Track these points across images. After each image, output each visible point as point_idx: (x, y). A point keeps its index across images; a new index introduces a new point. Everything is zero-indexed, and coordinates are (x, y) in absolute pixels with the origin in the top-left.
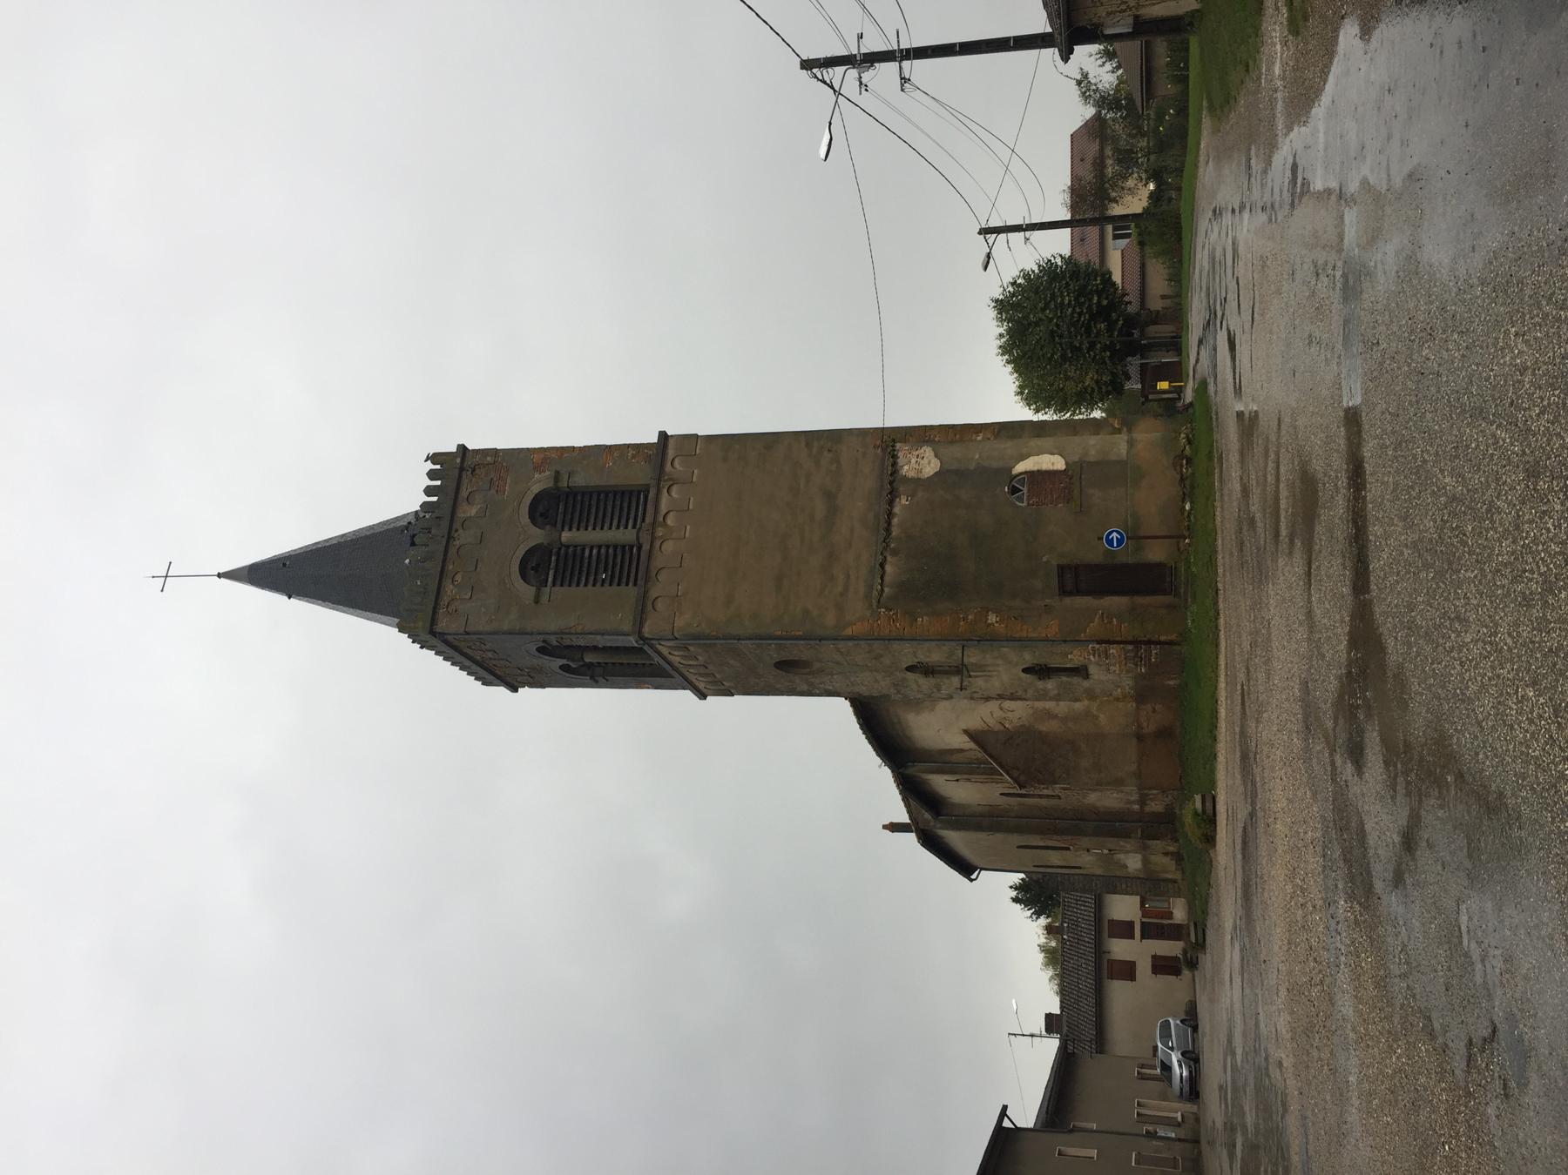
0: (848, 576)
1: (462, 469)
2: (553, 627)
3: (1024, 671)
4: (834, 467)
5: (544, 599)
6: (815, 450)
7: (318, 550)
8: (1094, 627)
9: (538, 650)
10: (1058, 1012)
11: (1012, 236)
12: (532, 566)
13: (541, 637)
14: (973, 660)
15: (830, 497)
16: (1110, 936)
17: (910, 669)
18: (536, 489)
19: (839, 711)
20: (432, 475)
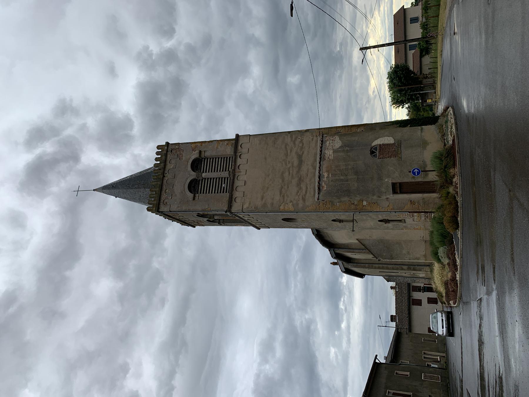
0: (307, 188)
1: (167, 151)
2: (200, 209)
4: (301, 145)
5: (197, 198)
6: (293, 139)
8: (408, 207)
10: (395, 315)
11: (372, 50)
12: (192, 184)
14: (358, 218)
16: (413, 305)
17: (334, 220)
18: (193, 157)
20: (157, 153)
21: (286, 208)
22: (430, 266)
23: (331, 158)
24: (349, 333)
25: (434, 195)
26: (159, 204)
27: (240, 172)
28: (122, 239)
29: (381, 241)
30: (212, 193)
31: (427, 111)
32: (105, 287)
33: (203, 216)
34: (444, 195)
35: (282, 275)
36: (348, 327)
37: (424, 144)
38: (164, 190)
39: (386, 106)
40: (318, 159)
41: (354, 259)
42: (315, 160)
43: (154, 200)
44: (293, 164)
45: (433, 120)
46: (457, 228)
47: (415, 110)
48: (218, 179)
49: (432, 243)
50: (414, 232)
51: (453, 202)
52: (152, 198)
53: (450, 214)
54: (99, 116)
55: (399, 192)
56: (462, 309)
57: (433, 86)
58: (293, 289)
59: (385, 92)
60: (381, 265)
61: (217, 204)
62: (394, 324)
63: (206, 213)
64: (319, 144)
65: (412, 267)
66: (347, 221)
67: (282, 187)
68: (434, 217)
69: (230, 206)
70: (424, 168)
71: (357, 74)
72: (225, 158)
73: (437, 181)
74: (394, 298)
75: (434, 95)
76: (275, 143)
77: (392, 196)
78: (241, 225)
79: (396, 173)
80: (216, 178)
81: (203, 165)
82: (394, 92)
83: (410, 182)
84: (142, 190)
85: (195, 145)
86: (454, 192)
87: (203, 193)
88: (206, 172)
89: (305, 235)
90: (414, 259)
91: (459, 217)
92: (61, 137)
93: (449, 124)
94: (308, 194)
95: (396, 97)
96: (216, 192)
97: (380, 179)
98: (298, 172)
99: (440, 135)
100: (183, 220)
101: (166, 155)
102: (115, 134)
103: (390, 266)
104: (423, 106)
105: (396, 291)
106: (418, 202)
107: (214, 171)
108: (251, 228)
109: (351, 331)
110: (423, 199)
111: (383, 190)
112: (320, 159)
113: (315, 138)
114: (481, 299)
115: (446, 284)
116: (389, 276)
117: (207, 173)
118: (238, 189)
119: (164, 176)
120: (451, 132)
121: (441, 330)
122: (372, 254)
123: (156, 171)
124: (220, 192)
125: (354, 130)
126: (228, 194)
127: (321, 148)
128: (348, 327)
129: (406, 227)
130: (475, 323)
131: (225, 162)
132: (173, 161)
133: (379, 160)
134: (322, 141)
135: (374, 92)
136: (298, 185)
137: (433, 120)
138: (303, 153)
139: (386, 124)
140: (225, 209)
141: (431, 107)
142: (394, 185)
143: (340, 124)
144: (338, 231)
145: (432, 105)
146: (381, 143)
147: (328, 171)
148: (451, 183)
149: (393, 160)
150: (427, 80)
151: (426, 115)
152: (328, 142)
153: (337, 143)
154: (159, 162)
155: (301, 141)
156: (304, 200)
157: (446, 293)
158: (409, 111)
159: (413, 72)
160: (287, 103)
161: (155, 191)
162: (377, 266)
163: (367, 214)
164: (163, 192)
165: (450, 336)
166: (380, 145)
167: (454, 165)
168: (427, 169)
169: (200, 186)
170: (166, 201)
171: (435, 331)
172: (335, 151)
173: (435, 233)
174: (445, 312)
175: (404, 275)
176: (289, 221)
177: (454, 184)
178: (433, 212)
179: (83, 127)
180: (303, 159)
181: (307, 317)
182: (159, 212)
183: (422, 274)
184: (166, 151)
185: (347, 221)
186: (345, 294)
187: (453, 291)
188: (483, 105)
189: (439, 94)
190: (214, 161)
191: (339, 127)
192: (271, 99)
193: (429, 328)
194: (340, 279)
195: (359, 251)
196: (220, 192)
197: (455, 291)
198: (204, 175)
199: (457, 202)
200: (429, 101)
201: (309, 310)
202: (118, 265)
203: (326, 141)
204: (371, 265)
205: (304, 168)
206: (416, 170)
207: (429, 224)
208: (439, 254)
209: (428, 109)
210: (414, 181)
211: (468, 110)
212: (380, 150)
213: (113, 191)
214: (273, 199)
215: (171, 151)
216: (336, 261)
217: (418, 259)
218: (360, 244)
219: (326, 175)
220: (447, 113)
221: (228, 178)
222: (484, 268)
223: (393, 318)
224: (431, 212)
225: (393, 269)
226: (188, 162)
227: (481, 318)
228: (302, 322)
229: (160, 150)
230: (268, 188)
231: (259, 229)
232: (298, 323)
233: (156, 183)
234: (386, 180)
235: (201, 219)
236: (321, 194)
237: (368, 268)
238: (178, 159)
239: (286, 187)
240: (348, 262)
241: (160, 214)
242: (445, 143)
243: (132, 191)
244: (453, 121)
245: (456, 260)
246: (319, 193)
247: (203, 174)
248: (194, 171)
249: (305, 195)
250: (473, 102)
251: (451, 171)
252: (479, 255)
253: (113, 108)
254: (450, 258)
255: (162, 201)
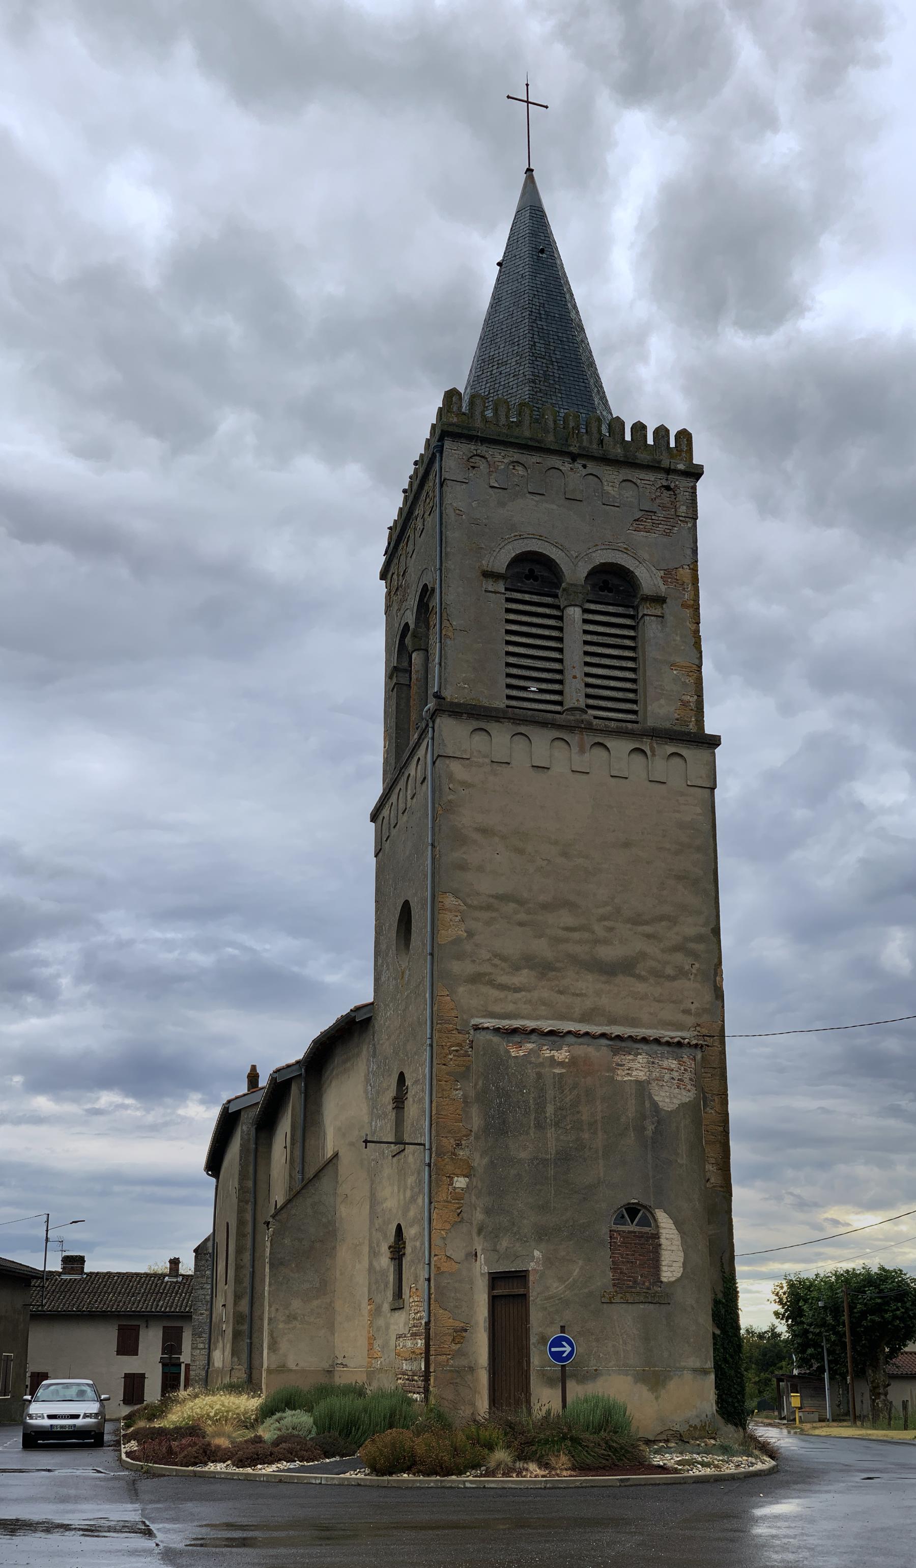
0: (517, 990)
1: (668, 471)
3: (399, 1228)
4: (669, 971)
5: (490, 585)
6: (692, 945)
7: (563, 295)
8: (446, 1321)
9: (425, 585)
13: (437, 586)
14: (411, 1159)
15: (625, 967)
16: (121, 1329)
17: (402, 1078)
19: (372, 1000)
20: (662, 432)
21: (448, 916)
22: (250, 1385)
23: (621, 1076)
24: (19, 1121)
25: (483, 1404)
26: (470, 438)
27: (582, 751)
28: (321, 286)
29: (330, 1233)
30: (508, 643)
31: (760, 1392)
32: (139, 210)
33: (424, 608)
34: (484, 1434)
35: (207, 897)
36: (38, 1120)
37: (654, 1378)
38: (523, 458)
39: (784, 1260)
40: (616, 1030)
41: (270, 1145)
42: (613, 1021)
43: (485, 420)
44: (606, 942)
45: (733, 1408)
46: (377, 1470)
47: (765, 1355)
48: (556, 666)
49: (324, 1391)
50: (364, 1335)
51: (461, 1461)
52: (496, 410)
53: (420, 1450)
54: (803, 185)
55: (496, 1292)
56: (115, 1478)
57: (846, 1414)
58: (158, 934)
59: (833, 1258)
60: (249, 1229)
61: (468, 664)
62: (55, 1265)
63: (435, 620)
64: (668, 1034)
65: (245, 1327)
66: (399, 1123)
67: (521, 902)
68: (411, 1402)
69: (457, 711)
70: (574, 1376)
71: (901, 1170)
72: (632, 695)
73: (530, 1413)
74: (142, 1268)
75: (816, 1416)
76: (679, 878)
77: (481, 1268)
78: (387, 752)
79: (558, 1285)
80: (561, 661)
81: (611, 609)
82: (831, 1286)
83: (527, 1331)
84: (526, 369)
85: (687, 579)
86: (492, 1464)
87: (508, 611)
88: (585, 621)
89: (349, 982)
90: (271, 1334)
91: (411, 1477)
92: (728, 17)
93: (718, 1458)
94: (495, 993)
95: (815, 1294)
96: (512, 660)
97: (542, 1234)
98: (574, 960)
99: (683, 1428)
100: (410, 532)
101: (654, 467)
102: (732, 251)
103: (247, 1257)
104: (780, 1380)
105: (164, 1275)
106: (460, 1353)
107: (586, 653)
108: (376, 789)
109: (25, 1129)
110: (472, 1369)
111: (504, 1243)
112: (618, 1037)
113: (690, 1020)
114: (148, 1533)
115: (193, 1430)
116: (214, 1256)
117: (579, 626)
118: (521, 742)
119: (574, 458)
120: (692, 1463)
121: (42, 1411)
122: (289, 1201)
123: (594, 425)
124: (509, 675)
125: (712, 1153)
126: (501, 703)
127: (657, 1041)
128: (38, 1120)
129: (376, 1312)
130: (73, 1512)
131: (620, 695)
132: (629, 494)
133: (605, 1230)
134: (679, 1044)
135: (836, 1222)
136: (529, 961)
137: (733, 1408)
138: (640, 978)
139: (726, 1256)
140: (448, 694)
141: (773, 1406)
142: (521, 1277)
143: (734, 1108)
144: (366, 1092)
145: (780, 1408)
146: (663, 1241)
147: (574, 1062)
148: (523, 1456)
149: (604, 1278)
150: (867, 1395)
151: (750, 1388)
152: (674, 1064)
153: (671, 1097)
154: (628, 437)
155: (681, 973)
156: (475, 979)
157: (162, 1432)
158: (761, 1336)
159: (895, 1352)
160: (815, 927)
161: (519, 424)
162: (249, 1217)
163: (421, 1191)
164: (515, 455)
165: (25, 1436)
166: (657, 1236)
167: (581, 1468)
168: (571, 1385)
169: (535, 598)
170: (483, 465)
171: (40, 1392)
172: (642, 1087)
173: (359, 1403)
174: (101, 1425)
175: (219, 1301)
176: (399, 924)
177: (519, 1465)
178: (426, 1399)
179: (761, 117)
180: (620, 979)
181: (65, 982)
182: (441, 439)
183: (220, 1357)
184: (667, 466)
185: (399, 1123)
186: (148, 1110)
187: (170, 1451)
188: (783, 1561)
189: (817, 1432)
190: (627, 653)
191: (725, 1103)
192: (831, 867)
193: (46, 1376)
194: (197, 1096)
195: (298, 1160)
196: (509, 675)
197: (169, 1457)
198: (574, 614)
199: (460, 1473)
200: (795, 1400)
201: (86, 988)
202: (225, 264)
203: (678, 1058)
204: (250, 1197)
205: (588, 983)
206: (568, 1349)
207: (388, 1383)
208: (289, 1413)
209: (767, 1395)
210: (533, 1339)
211: (764, 1518)
212: (641, 1236)
213: (525, 249)
214: (480, 869)
215: (668, 488)
216: (263, 1082)
217: (273, 1347)
218: (322, 1162)
219: (562, 1055)
220: (757, 1452)
221: (560, 703)
222: (244, 1546)
223: (74, 1263)
224: (427, 1391)
225: (238, 1268)
226: (625, 551)
227: (91, 1531)
228: (45, 963)
229: (672, 444)
230: (521, 852)
231: (374, 817)
232: (42, 949)
233: (551, 424)
234: (537, 1253)
235: (413, 602)
236: (496, 1039)
237: (242, 1189)
238: (638, 515)
239: (522, 916)
240: (263, 1123)
241: (434, 443)
242: (654, 1442)
243: (524, 328)
244: (729, 1469)
245: (271, 1463)
246: (497, 1030)
247: (578, 610)
248: (592, 573)
249: (491, 983)
250: (791, 1532)
251: (564, 1458)
252: (291, 1533)
253: (830, 244)
254: (276, 1443)
255: (483, 449)
